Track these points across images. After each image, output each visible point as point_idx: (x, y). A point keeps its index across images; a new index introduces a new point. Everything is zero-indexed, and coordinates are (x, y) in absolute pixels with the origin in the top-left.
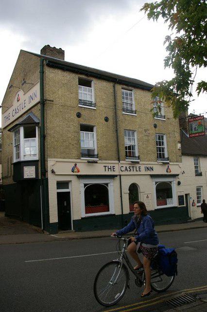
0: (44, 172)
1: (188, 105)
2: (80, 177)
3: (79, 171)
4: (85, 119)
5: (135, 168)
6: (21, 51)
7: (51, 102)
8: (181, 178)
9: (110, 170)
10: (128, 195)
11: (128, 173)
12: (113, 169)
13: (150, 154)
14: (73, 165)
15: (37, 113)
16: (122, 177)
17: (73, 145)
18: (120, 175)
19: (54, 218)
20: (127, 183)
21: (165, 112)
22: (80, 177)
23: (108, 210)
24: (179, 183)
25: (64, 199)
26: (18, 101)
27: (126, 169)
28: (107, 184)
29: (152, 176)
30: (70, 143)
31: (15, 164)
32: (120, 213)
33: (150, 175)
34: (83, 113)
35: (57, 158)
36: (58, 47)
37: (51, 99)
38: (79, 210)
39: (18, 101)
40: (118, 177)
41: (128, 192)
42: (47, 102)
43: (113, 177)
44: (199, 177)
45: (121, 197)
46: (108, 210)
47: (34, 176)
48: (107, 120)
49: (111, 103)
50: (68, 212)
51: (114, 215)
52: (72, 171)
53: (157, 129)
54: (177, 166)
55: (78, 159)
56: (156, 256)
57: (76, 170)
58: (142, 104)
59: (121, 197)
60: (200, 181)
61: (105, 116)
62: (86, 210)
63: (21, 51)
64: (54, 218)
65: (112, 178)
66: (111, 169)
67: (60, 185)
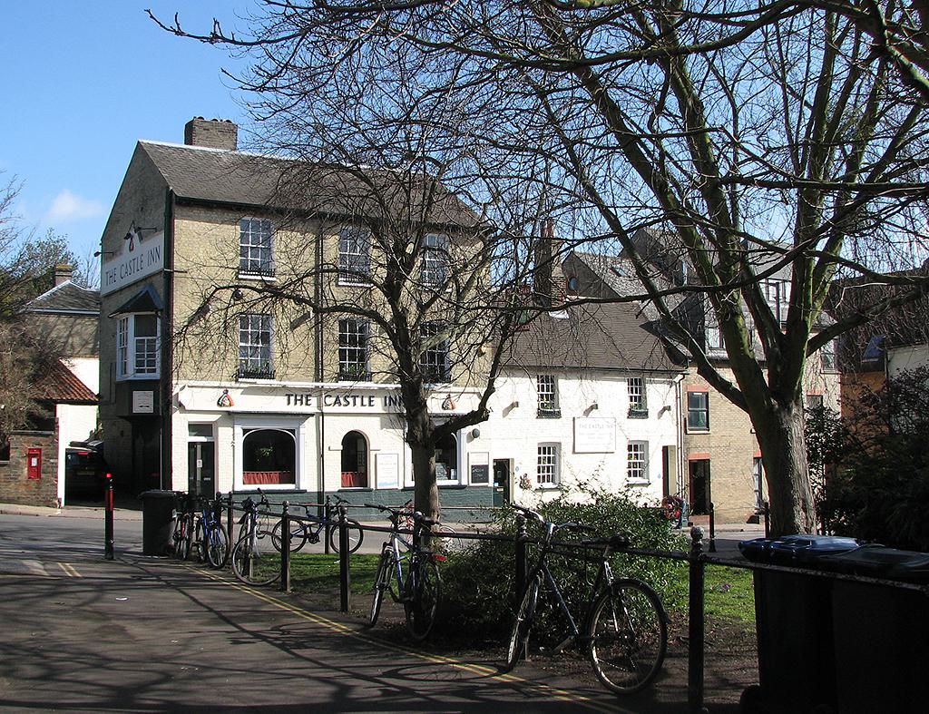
0: (168, 405)
5: (358, 400)
6: (189, 443)
9: (299, 402)
10: (339, 455)
11: (337, 409)
15: (159, 283)
19: (180, 482)
20: (337, 431)
25: (204, 455)
26: (131, 250)
31: (119, 385)
38: (230, 476)
39: (131, 250)
41: (341, 448)
44: (552, 421)
47: (151, 410)
50: (154, 475)
56: (436, 615)
60: (550, 431)
62: (488, 469)
63: (189, 443)
64: (180, 482)
67: (195, 428)
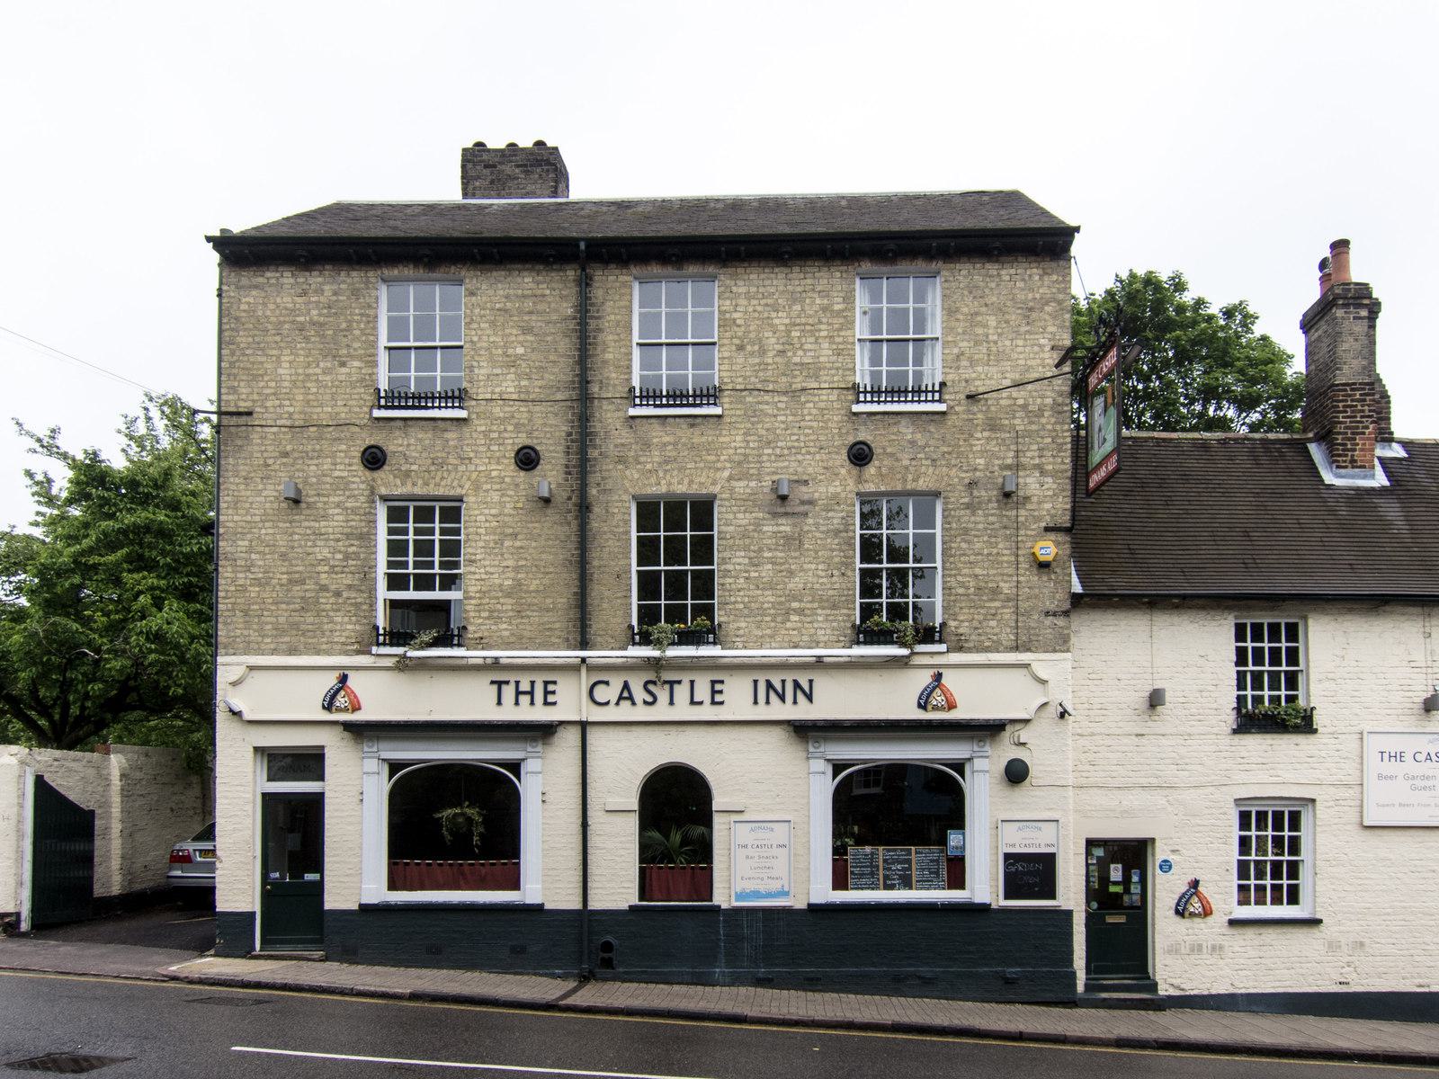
1: (1132, 276)
2: (362, 732)
3: (356, 707)
4: (407, 474)
7: (242, 420)
8: (1040, 750)
11: (625, 712)
12: (546, 693)
13: (800, 612)
14: (331, 680)
16: (594, 736)
17: (338, 594)
18: (584, 726)
21: (953, 362)
22: (362, 732)
23: (515, 885)
24: (1016, 774)
27: (626, 695)
28: (515, 767)
29: (804, 731)
30: (324, 588)
32: (575, 904)
33: (788, 723)
34: (394, 444)
35: (260, 652)
36: (526, 142)
37: (244, 406)
40: (570, 738)
42: (625, 395)
43: (544, 732)
45: (585, 825)
46: (515, 885)
48: (527, 459)
49: (560, 370)
51: (538, 909)
52: (920, 706)
53: (871, 470)
54: (1024, 671)
55: (358, 652)
57: (938, 698)
58: (772, 341)
59: (585, 825)
61: (522, 440)
65: (534, 740)
66: (531, 693)
67: (284, 762)
